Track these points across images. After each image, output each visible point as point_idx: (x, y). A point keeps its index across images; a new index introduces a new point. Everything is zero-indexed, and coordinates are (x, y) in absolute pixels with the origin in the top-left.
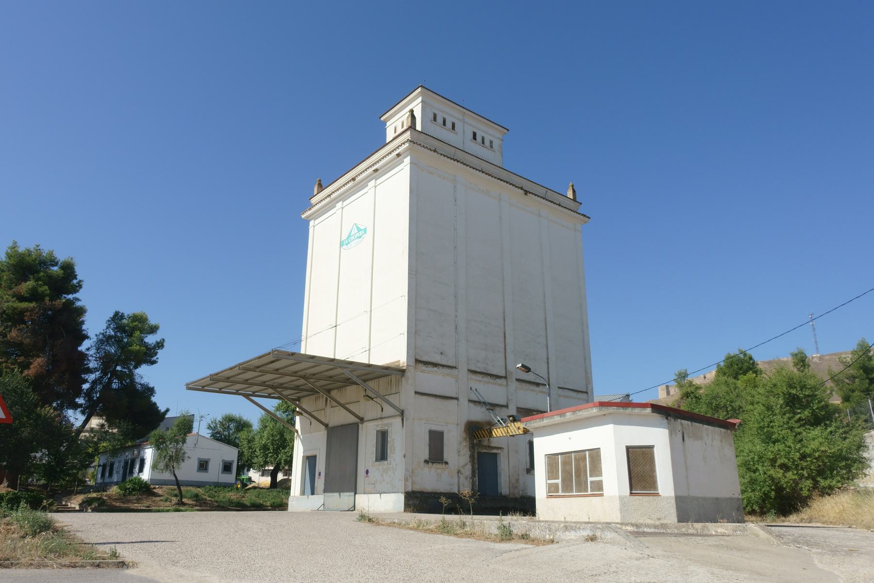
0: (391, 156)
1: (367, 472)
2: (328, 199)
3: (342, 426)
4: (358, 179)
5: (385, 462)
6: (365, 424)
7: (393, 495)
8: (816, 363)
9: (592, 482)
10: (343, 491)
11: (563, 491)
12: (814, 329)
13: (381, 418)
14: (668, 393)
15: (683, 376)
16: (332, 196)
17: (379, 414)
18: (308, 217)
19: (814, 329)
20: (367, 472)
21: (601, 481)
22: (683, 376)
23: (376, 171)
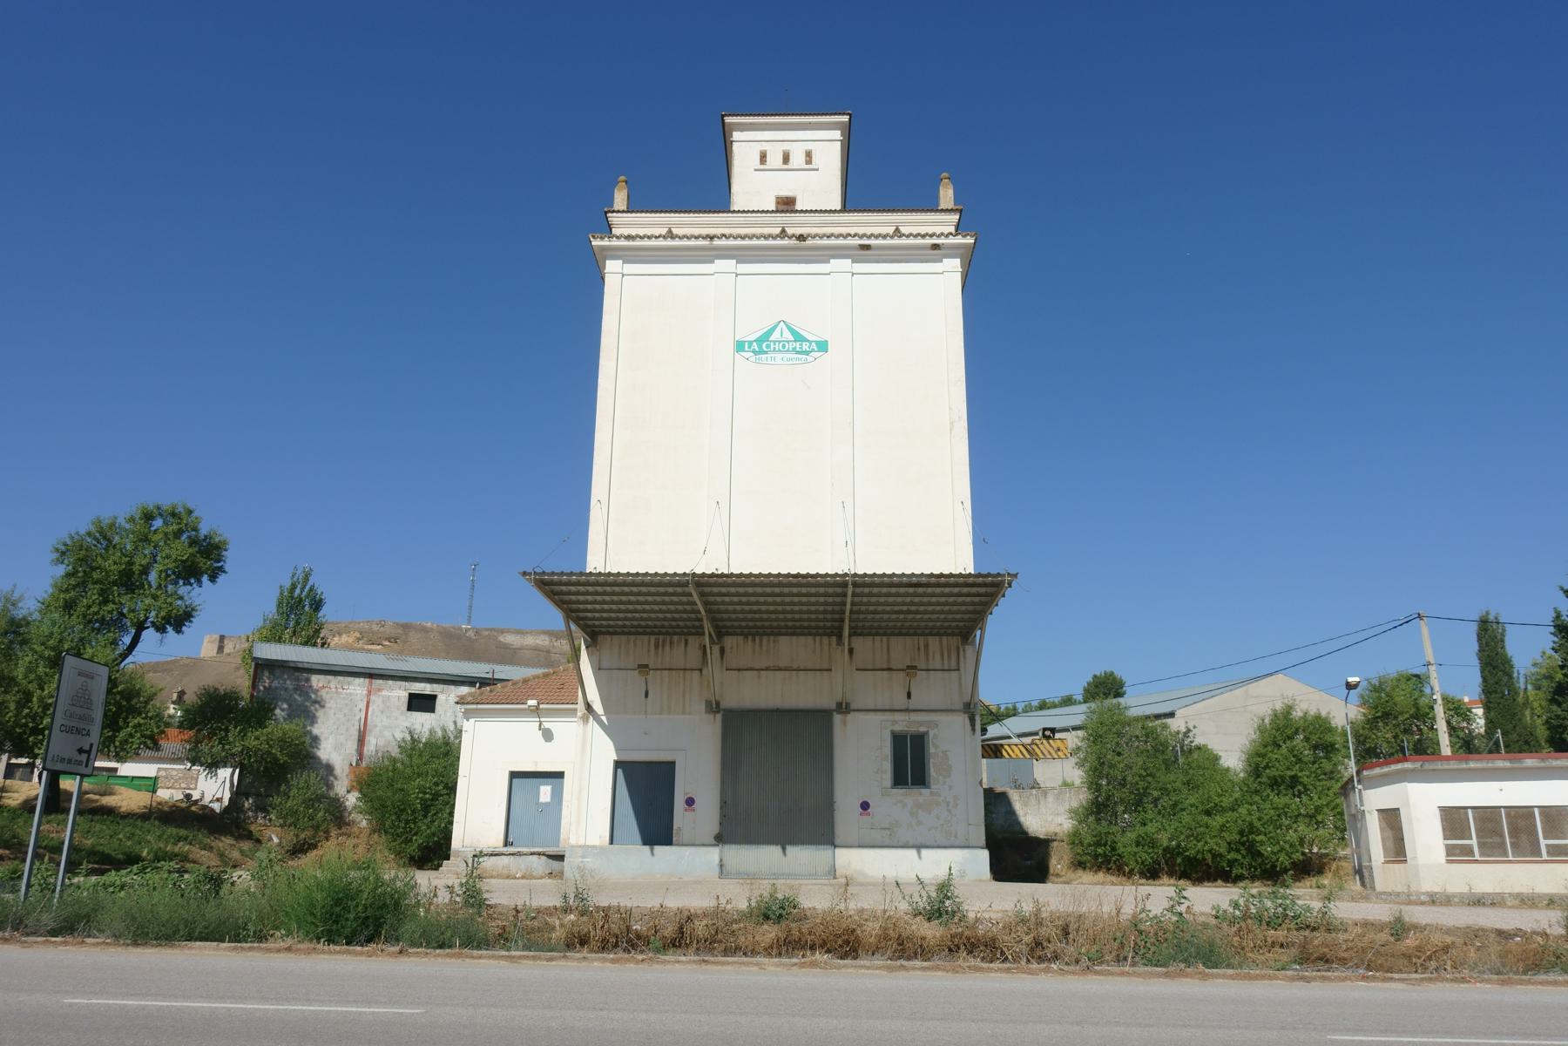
0: (919, 241)
1: (865, 806)
2: (706, 243)
3: (777, 711)
4: (809, 242)
5: (925, 791)
6: (851, 717)
7: (966, 851)
8: (469, 639)
9: (1548, 846)
10: (794, 842)
11: (1481, 855)
12: (473, 587)
13: (907, 710)
14: (221, 649)
15: (1106, 687)
16: (717, 242)
17: (900, 701)
18: (603, 248)
19: (473, 587)
20: (865, 806)
21: (1445, 838)
22: (1106, 687)
23: (868, 247)
